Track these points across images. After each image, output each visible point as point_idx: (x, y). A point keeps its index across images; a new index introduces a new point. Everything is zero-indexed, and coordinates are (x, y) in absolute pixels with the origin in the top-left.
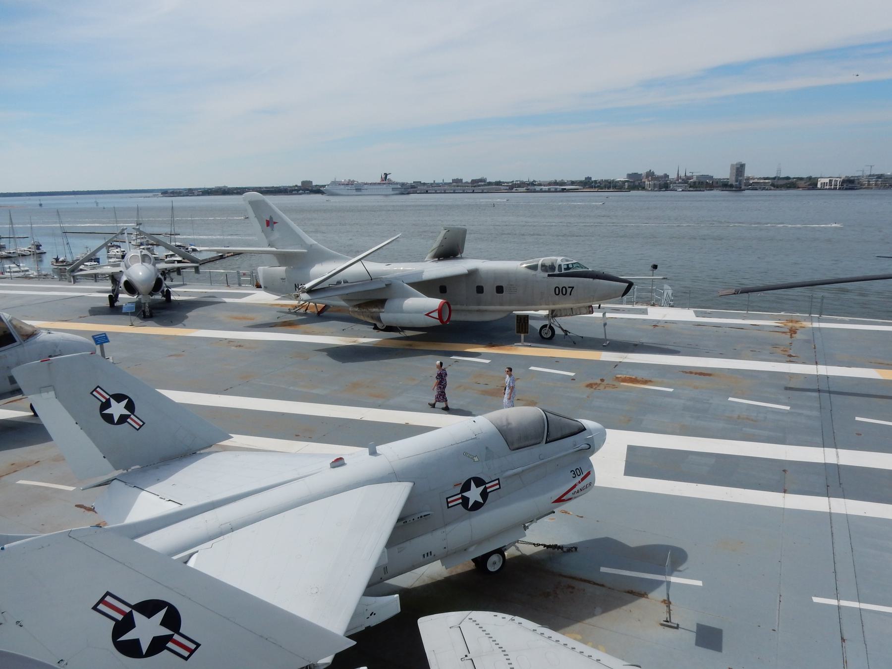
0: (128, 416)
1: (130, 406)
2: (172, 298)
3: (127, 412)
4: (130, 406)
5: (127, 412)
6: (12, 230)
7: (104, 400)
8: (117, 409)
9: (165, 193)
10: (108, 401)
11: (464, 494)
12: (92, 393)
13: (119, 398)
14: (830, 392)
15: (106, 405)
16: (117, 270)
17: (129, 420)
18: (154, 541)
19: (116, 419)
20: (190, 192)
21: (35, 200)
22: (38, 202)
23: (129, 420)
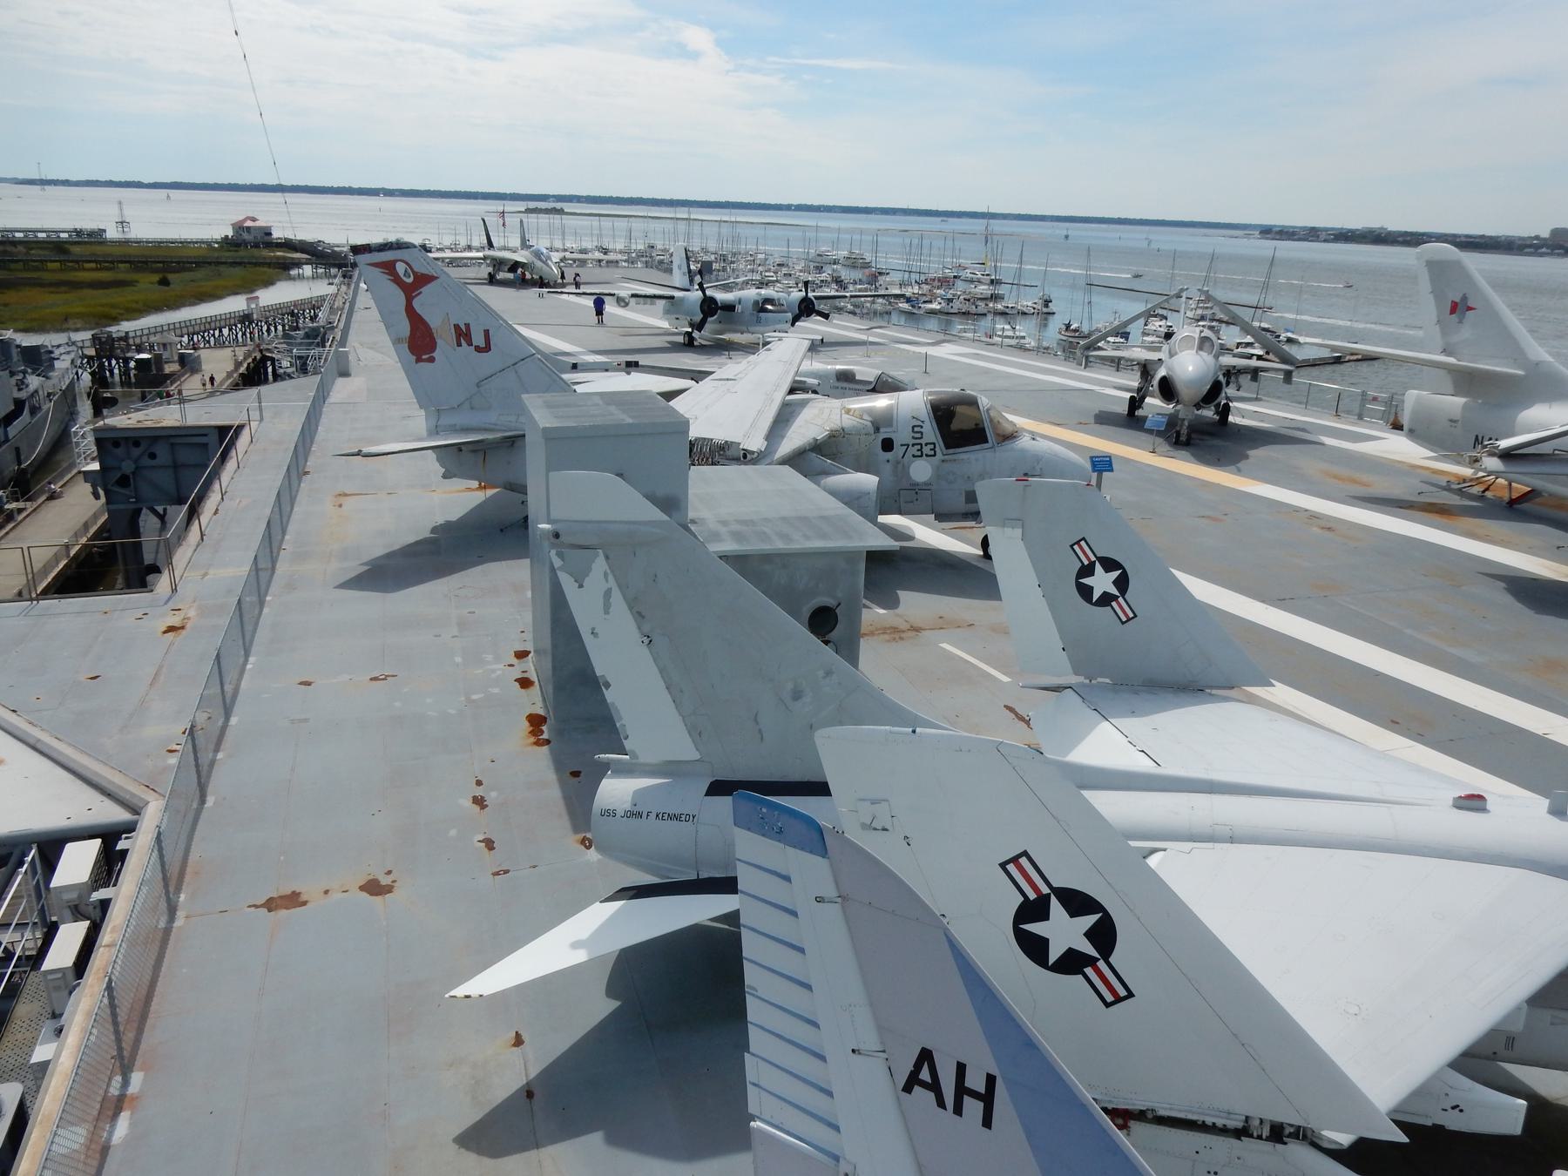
0: (1115, 598)
1: (1122, 583)
4: (1122, 583)
8: (1102, 582)
9: (1267, 232)
13: (1109, 564)
15: (1087, 570)
20: (1312, 234)
21: (978, 226)
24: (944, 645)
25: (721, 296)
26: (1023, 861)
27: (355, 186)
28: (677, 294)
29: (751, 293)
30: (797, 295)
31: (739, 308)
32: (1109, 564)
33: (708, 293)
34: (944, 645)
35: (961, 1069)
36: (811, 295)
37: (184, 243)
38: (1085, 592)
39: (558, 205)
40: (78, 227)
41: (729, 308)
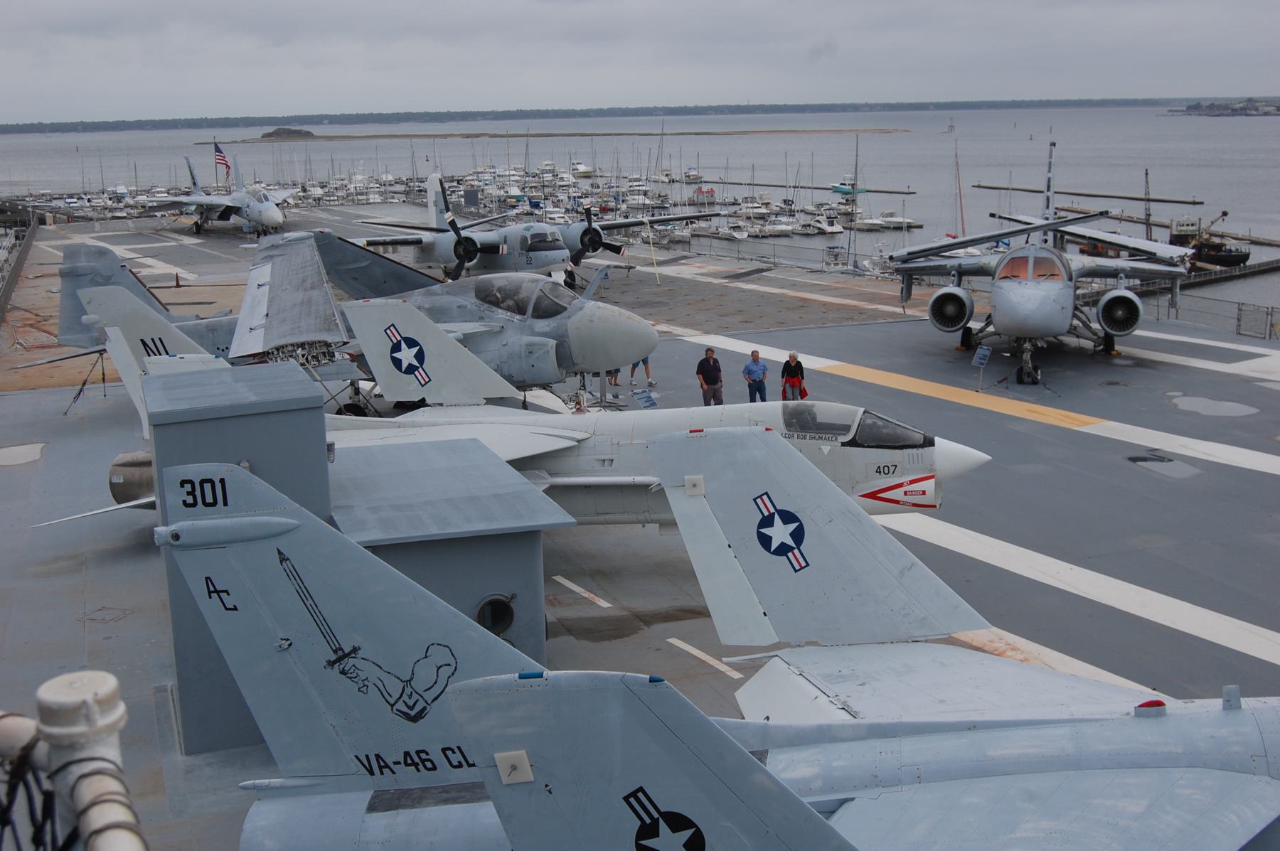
0: (791, 549)
1: (798, 535)
2: (1117, 347)
3: (790, 542)
4: (798, 535)
5: (790, 542)
6: (1044, 229)
7: (766, 514)
8: (780, 533)
10: (771, 516)
11: (777, 517)
12: (755, 500)
13: (788, 517)
14: (527, 154)
15: (767, 521)
16: (431, 197)
17: (790, 555)
18: (789, 768)
19: (774, 546)
22: (234, 194)
23: (790, 555)
24: (674, 641)
25: (480, 236)
26: (640, 795)
27: (47, 121)
28: (426, 237)
29: (516, 229)
30: (578, 227)
31: (504, 249)
32: (788, 517)
33: (464, 233)
34: (674, 641)
35: (367, 756)
36: (595, 225)
37: (590, 619)
38: (765, 541)
39: (305, 128)
40: (1250, 95)
41: (491, 250)
